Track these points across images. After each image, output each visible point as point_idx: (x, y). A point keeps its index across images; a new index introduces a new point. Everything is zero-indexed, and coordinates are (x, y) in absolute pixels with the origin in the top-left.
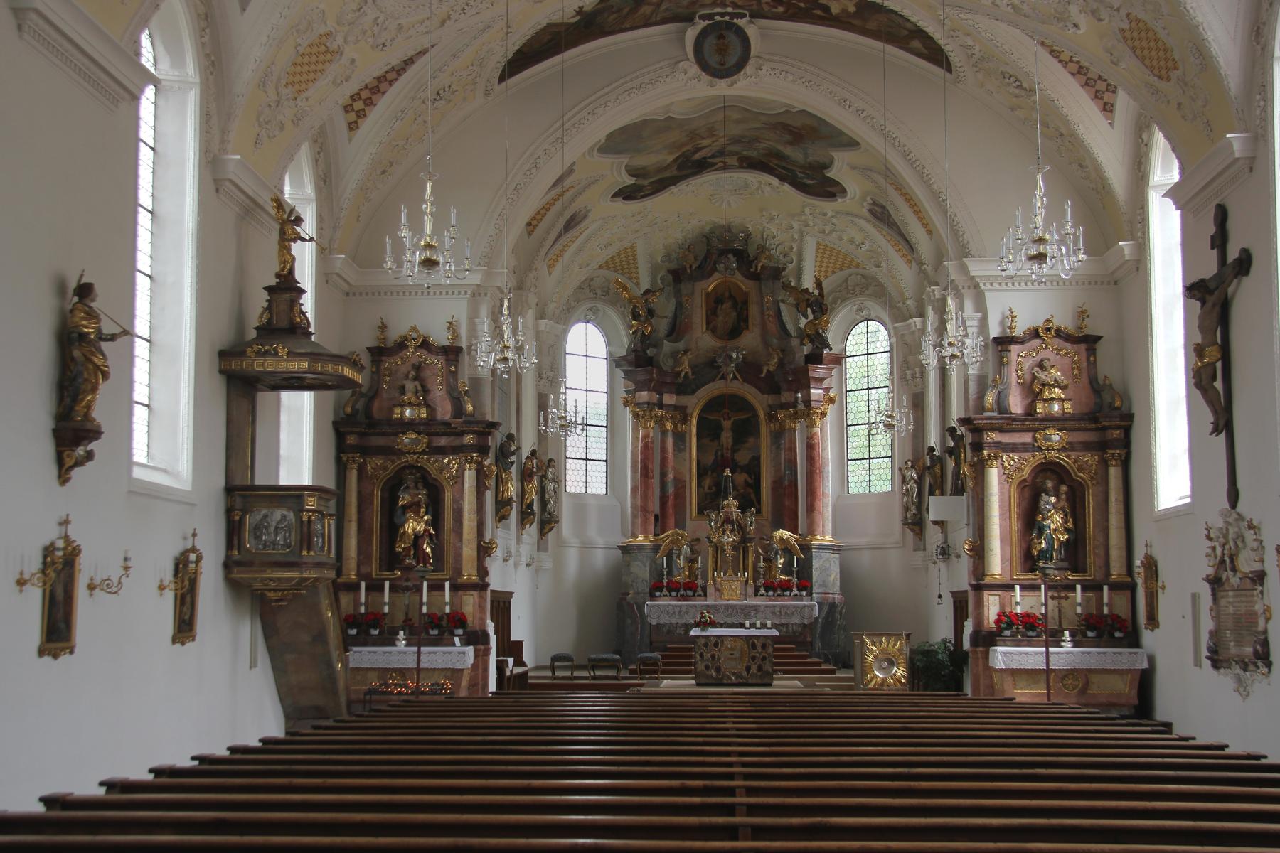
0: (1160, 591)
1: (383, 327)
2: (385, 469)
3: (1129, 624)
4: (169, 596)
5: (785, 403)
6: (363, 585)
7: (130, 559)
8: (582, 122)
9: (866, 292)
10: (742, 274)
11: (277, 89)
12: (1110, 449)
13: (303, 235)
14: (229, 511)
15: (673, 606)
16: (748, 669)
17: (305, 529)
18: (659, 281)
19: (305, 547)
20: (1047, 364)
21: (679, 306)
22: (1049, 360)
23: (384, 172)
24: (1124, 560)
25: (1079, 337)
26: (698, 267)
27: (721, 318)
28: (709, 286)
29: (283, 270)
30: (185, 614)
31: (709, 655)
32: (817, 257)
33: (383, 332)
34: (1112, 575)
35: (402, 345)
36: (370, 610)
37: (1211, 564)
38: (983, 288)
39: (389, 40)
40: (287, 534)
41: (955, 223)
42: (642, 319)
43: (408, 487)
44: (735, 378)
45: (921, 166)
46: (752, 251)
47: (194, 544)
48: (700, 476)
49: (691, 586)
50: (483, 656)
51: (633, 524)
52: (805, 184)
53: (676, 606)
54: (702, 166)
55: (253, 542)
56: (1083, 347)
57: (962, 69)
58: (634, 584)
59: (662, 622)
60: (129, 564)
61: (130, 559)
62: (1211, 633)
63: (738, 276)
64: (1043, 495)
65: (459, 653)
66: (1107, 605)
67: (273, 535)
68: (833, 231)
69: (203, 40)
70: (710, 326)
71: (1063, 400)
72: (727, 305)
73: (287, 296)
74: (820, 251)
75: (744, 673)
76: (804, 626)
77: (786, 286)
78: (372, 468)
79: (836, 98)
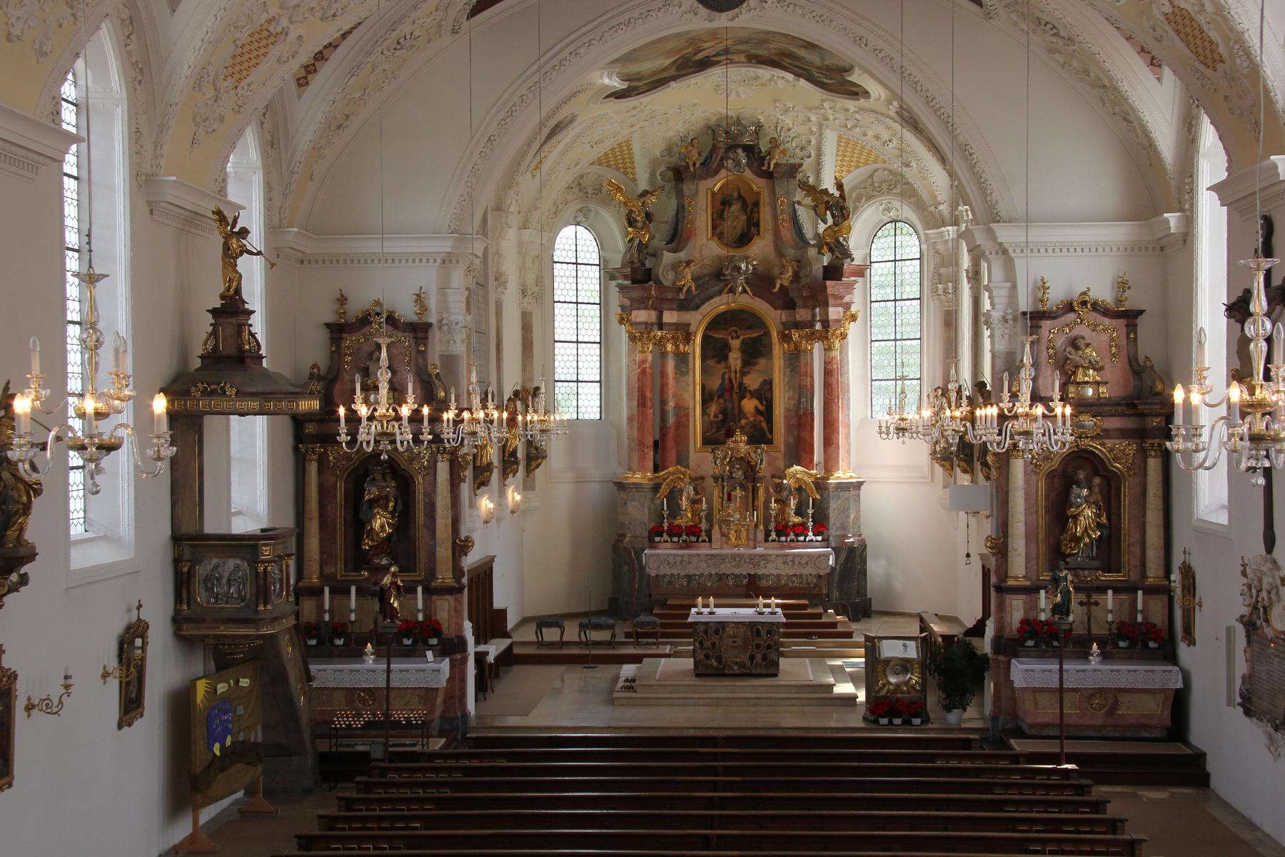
0: (1197, 607)
1: (342, 300)
3: (1165, 635)
4: (114, 684)
5: (800, 322)
6: (327, 590)
7: (70, 677)
8: (564, 63)
9: (894, 191)
11: (214, 84)
12: (1148, 438)
13: (249, 247)
14: (177, 561)
15: (674, 555)
16: (752, 658)
17: (261, 581)
18: (659, 178)
19: (261, 601)
20: (1081, 343)
21: (681, 209)
22: (1083, 338)
23: (339, 127)
24: (1161, 562)
25: (1115, 311)
26: (702, 164)
28: (716, 185)
29: (229, 287)
30: (132, 692)
31: (709, 643)
32: (838, 151)
33: (342, 305)
34: (1148, 577)
35: (364, 320)
36: (336, 620)
37: (1247, 602)
38: (1012, 255)
39: (340, 9)
40: (241, 587)
41: (983, 180)
43: (374, 479)
44: (745, 291)
45: (946, 115)
46: (764, 146)
47: (139, 616)
48: (706, 401)
49: (694, 531)
50: (460, 664)
51: (630, 458)
52: (823, 83)
53: (678, 555)
54: (705, 64)
55: (204, 594)
56: (1122, 322)
57: (993, 8)
58: (632, 527)
59: (661, 573)
60: (69, 682)
61: (70, 677)
62: (1243, 677)
63: (748, 174)
64: (1075, 486)
65: (434, 671)
66: (1142, 612)
67: (225, 587)
68: (855, 126)
69: (128, 48)
70: (717, 231)
71: (1098, 383)
72: (735, 208)
73: (233, 320)
74: (842, 144)
75: (748, 663)
76: (820, 577)
77: (804, 185)
78: (334, 458)
79: (851, 35)
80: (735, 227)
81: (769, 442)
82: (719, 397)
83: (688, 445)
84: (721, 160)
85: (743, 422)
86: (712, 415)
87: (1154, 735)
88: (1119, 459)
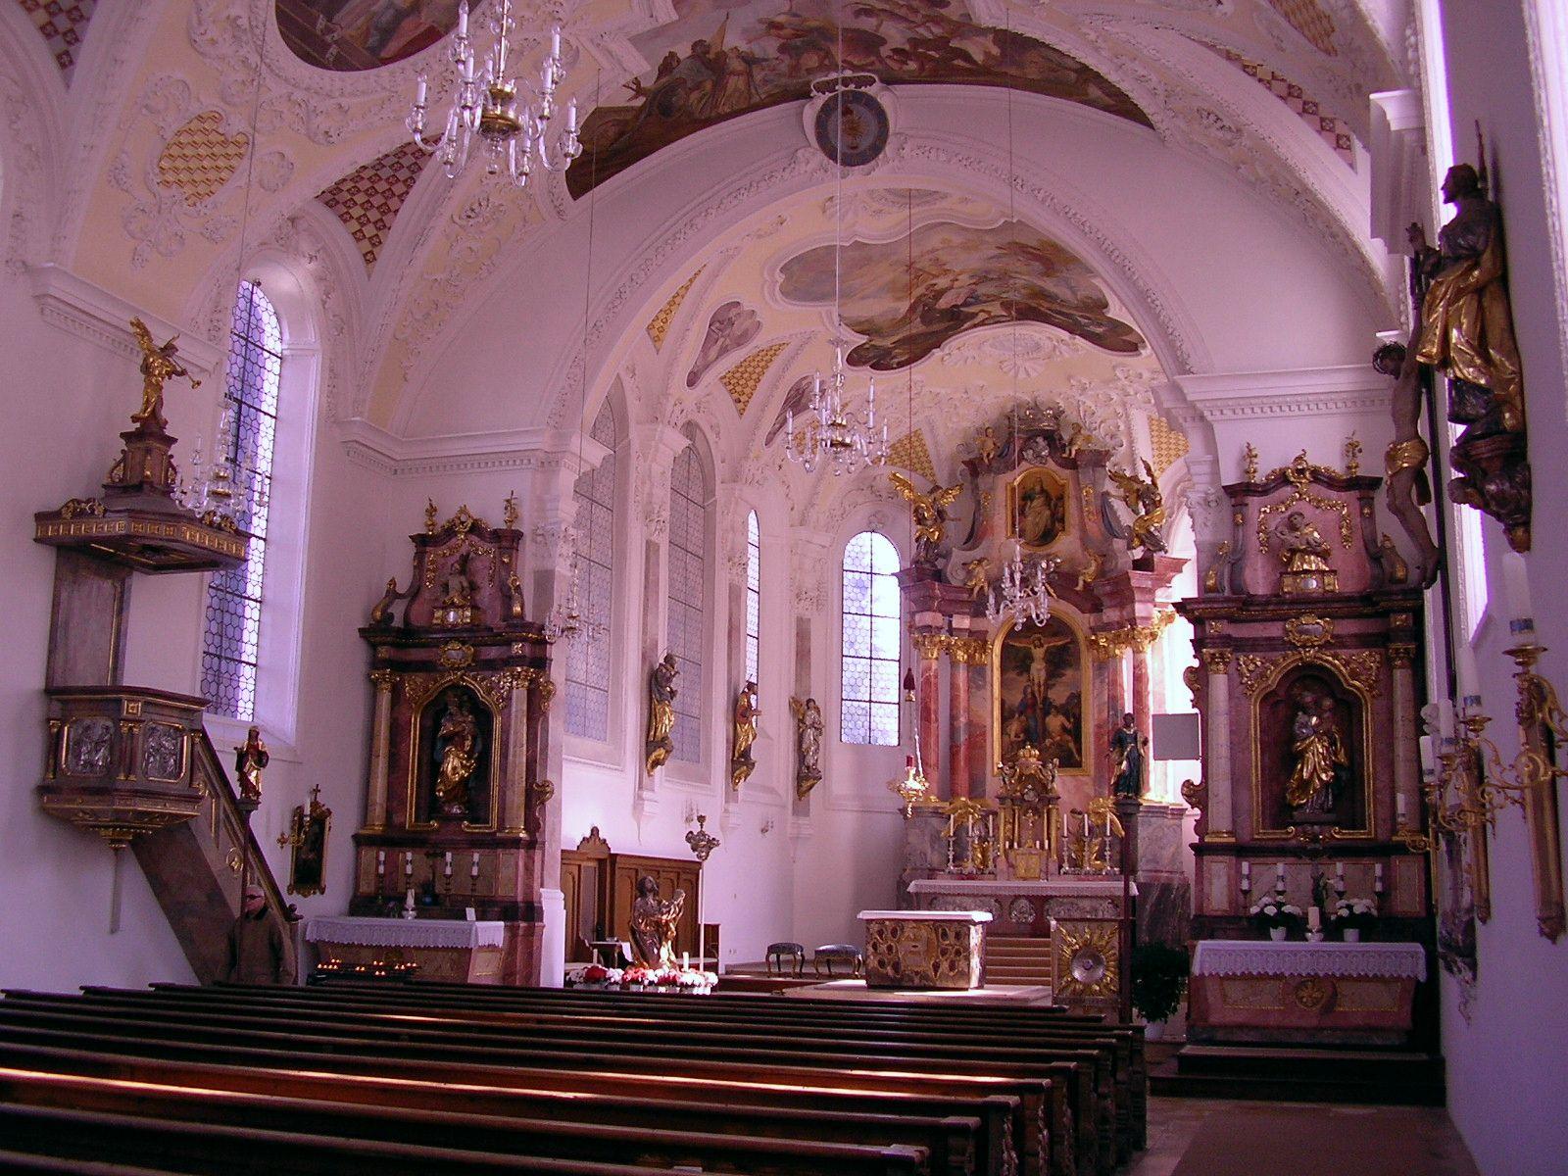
1: (432, 511)
2: (426, 690)
8: (678, 236)
10: (1056, 462)
16: (936, 967)
27: (1030, 518)
35: (450, 532)
38: (1209, 418)
41: (1170, 330)
42: (929, 523)
48: (1006, 718)
54: (956, 320)
56: (1355, 494)
63: (1051, 464)
66: (1381, 879)
70: (1017, 529)
72: (1038, 502)
78: (412, 689)
80: (1037, 524)
81: (1078, 765)
82: (1021, 713)
83: (985, 765)
84: (1021, 451)
85: (1048, 742)
86: (1012, 736)
87: (1388, 1043)
88: (1358, 674)
